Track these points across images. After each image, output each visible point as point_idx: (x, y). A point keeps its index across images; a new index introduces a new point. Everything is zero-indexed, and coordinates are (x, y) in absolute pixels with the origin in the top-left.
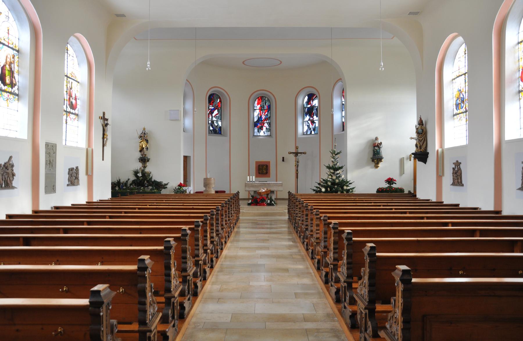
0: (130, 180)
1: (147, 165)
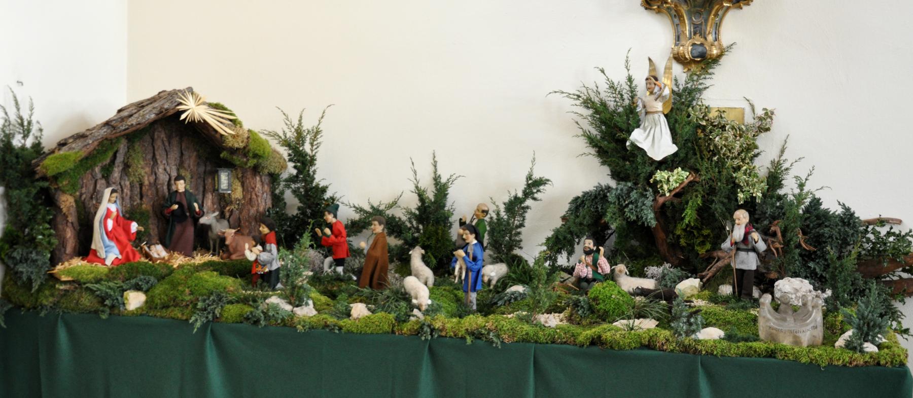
0: (545, 193)
1: (725, 40)
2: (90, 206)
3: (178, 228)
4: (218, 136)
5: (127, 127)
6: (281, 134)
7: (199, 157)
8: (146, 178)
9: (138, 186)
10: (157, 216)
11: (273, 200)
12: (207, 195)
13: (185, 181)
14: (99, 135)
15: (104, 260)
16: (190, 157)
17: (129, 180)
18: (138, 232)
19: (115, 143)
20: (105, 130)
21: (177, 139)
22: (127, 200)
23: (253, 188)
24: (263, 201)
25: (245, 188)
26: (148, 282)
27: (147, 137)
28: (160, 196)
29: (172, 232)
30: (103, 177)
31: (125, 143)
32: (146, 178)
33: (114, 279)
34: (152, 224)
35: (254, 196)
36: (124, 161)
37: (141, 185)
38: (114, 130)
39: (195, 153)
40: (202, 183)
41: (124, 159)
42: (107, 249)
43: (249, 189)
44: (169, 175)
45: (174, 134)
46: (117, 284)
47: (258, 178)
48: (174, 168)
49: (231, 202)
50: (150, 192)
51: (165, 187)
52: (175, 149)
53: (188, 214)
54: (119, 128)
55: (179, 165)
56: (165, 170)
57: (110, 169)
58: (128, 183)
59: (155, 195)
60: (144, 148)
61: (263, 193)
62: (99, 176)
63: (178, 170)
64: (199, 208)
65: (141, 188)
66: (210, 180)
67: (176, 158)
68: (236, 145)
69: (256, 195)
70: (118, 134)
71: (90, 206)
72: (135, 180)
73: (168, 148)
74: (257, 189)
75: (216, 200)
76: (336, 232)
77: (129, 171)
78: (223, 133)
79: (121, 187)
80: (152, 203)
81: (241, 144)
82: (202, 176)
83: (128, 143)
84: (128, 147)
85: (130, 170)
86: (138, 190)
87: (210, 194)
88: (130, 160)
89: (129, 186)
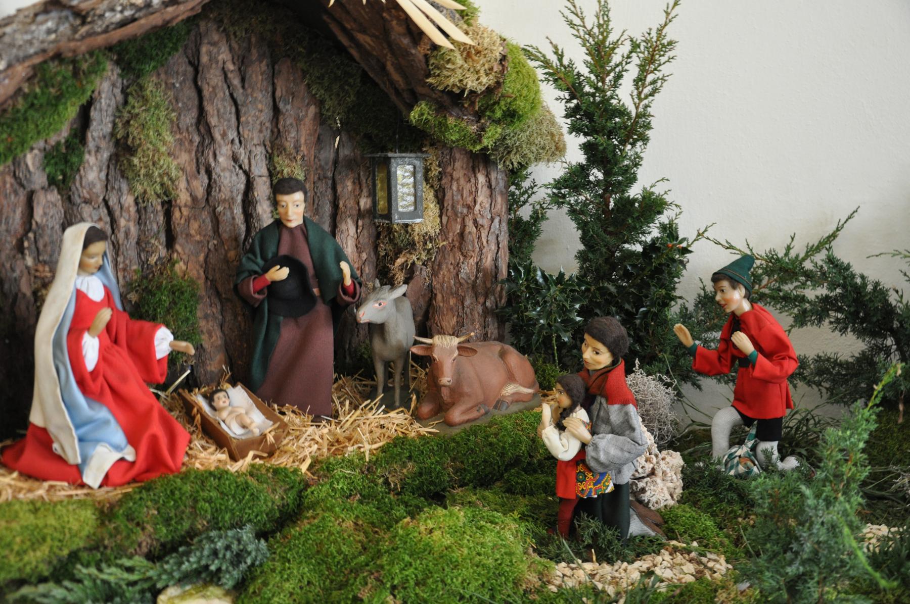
2: (16, 274)
3: (288, 334)
4: (420, 51)
5: (128, 13)
6: (612, 38)
7: (322, 119)
8: (182, 185)
9: (159, 208)
10: (218, 294)
11: (512, 235)
12: (343, 227)
13: (305, 193)
14: (30, 42)
15: (78, 470)
16: (299, 120)
17: (131, 190)
18: (173, 358)
19: (87, 74)
20: (50, 24)
21: (264, 66)
22: (130, 251)
23: (469, 207)
24: (492, 239)
25: (448, 202)
26: (239, 558)
27: (179, 61)
28: (225, 236)
29: (269, 346)
30: (52, 181)
31: (114, 77)
32: (182, 185)
33: (121, 551)
34: (206, 317)
35: (471, 227)
36: (113, 134)
37: (168, 206)
38: (84, 23)
39: (312, 110)
40: (329, 193)
41: (115, 125)
42: (83, 430)
43: (460, 208)
44: (247, 174)
45: (254, 51)
46: (130, 570)
47: (481, 179)
48: (259, 151)
49: (412, 245)
50: (195, 225)
51: (238, 211)
52: (259, 95)
53: (316, 291)
54: (101, 16)
55: (272, 143)
56: (235, 159)
57: (74, 159)
58: (128, 200)
59: (211, 233)
60: (171, 93)
61: (492, 220)
62: (39, 179)
63: (270, 158)
64: (352, 276)
65: (168, 215)
66: (349, 185)
67: (262, 124)
68: (471, 83)
69: (475, 222)
70: (100, 40)
71: (16, 274)
72: (150, 191)
73: (239, 94)
74: (477, 207)
75: (365, 239)
76: (766, 344)
77: (131, 165)
78: (439, 39)
79: (110, 213)
80: (202, 257)
81: (484, 80)
82: (330, 174)
83: (121, 76)
84: (124, 91)
85: (136, 161)
86: (161, 218)
87: (349, 221)
88: (134, 130)
89: (133, 209)
